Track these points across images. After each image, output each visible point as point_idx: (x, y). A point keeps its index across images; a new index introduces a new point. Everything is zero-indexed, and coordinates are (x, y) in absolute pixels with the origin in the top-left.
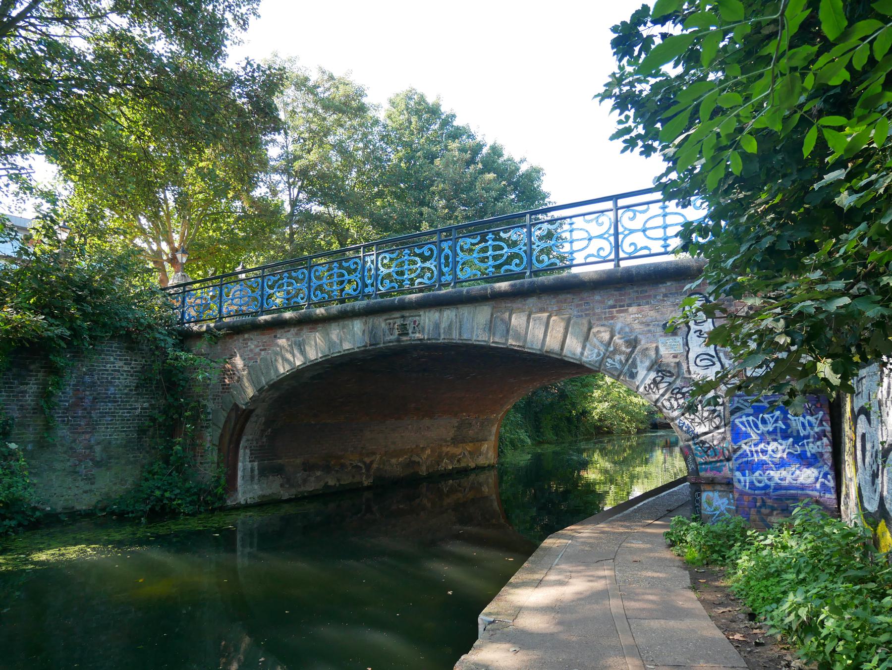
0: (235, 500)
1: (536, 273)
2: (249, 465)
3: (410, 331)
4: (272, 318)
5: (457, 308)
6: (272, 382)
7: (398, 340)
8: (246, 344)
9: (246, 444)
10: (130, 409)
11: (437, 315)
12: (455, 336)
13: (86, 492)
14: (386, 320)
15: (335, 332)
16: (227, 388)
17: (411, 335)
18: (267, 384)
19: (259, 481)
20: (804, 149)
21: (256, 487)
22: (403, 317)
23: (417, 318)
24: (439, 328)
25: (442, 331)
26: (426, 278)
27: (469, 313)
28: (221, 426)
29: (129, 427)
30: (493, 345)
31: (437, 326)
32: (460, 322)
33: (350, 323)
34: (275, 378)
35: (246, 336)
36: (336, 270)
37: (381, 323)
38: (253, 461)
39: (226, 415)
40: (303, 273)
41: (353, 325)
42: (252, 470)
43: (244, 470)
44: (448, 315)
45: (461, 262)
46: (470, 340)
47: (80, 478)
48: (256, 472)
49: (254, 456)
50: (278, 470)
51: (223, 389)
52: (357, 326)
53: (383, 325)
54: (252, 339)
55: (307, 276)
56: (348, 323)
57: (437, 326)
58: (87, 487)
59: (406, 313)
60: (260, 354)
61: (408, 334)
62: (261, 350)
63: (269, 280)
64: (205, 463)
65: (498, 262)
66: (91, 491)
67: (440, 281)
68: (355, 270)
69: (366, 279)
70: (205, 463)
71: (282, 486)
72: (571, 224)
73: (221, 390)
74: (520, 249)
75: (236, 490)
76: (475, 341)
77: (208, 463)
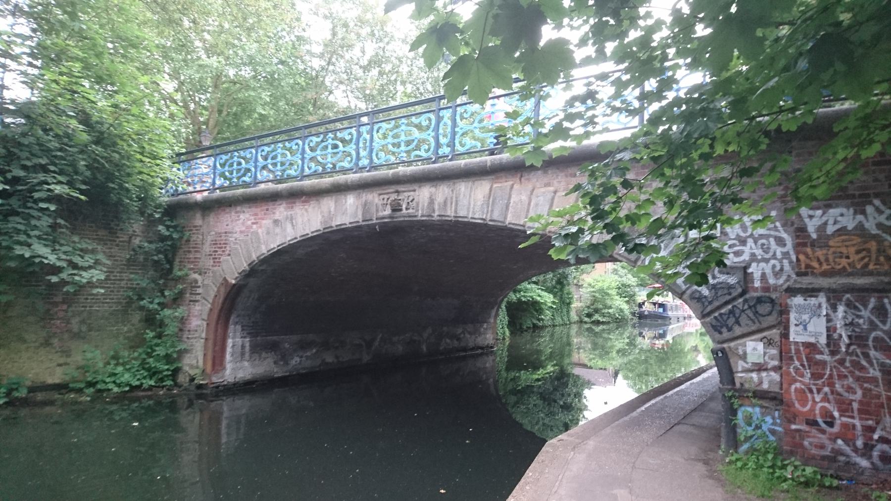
0: (222, 377)
1: (456, 156)
2: (239, 341)
3: (404, 207)
4: (318, 182)
5: (317, 200)
6: (262, 257)
7: (390, 217)
8: (239, 216)
9: (237, 320)
10: (114, 280)
11: (433, 190)
12: (450, 213)
13: (60, 365)
14: (380, 194)
15: (328, 204)
16: (218, 262)
17: (404, 211)
18: (258, 258)
19: (251, 357)
20: (606, 50)
21: (246, 364)
22: (397, 192)
23: (412, 193)
24: (433, 203)
25: (436, 207)
26: (422, 150)
27: (466, 188)
28: (211, 301)
29: (113, 299)
30: (491, 223)
31: (432, 201)
32: (456, 198)
33: (343, 197)
34: (265, 251)
35: (239, 208)
36: (330, 141)
37: (374, 198)
38: (245, 337)
39: (216, 289)
40: (297, 144)
41: (346, 200)
42: (243, 347)
43: (233, 346)
44: (442, 192)
45: (461, 132)
46: (466, 217)
47: (54, 351)
48: (247, 348)
49: (245, 332)
50: (273, 347)
51: (214, 262)
52: (351, 201)
53: (376, 200)
54: (244, 212)
55: (254, 155)
56: (342, 197)
57: (432, 201)
58: (62, 361)
59: (401, 188)
60: (251, 227)
61: (401, 210)
62: (253, 223)
63: (263, 151)
64: (192, 338)
65: (410, 148)
66: (66, 364)
67: (358, 165)
68: (251, 159)
69: (441, 137)
70: (192, 338)
71: (275, 363)
72: (493, 105)
73: (212, 263)
74: (429, 135)
75: (224, 368)
76: (472, 218)
77: (195, 338)
